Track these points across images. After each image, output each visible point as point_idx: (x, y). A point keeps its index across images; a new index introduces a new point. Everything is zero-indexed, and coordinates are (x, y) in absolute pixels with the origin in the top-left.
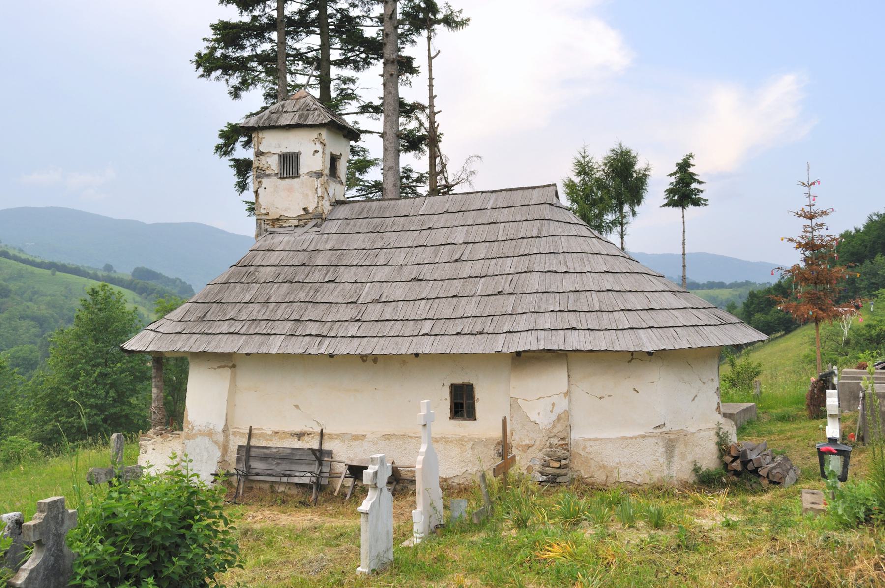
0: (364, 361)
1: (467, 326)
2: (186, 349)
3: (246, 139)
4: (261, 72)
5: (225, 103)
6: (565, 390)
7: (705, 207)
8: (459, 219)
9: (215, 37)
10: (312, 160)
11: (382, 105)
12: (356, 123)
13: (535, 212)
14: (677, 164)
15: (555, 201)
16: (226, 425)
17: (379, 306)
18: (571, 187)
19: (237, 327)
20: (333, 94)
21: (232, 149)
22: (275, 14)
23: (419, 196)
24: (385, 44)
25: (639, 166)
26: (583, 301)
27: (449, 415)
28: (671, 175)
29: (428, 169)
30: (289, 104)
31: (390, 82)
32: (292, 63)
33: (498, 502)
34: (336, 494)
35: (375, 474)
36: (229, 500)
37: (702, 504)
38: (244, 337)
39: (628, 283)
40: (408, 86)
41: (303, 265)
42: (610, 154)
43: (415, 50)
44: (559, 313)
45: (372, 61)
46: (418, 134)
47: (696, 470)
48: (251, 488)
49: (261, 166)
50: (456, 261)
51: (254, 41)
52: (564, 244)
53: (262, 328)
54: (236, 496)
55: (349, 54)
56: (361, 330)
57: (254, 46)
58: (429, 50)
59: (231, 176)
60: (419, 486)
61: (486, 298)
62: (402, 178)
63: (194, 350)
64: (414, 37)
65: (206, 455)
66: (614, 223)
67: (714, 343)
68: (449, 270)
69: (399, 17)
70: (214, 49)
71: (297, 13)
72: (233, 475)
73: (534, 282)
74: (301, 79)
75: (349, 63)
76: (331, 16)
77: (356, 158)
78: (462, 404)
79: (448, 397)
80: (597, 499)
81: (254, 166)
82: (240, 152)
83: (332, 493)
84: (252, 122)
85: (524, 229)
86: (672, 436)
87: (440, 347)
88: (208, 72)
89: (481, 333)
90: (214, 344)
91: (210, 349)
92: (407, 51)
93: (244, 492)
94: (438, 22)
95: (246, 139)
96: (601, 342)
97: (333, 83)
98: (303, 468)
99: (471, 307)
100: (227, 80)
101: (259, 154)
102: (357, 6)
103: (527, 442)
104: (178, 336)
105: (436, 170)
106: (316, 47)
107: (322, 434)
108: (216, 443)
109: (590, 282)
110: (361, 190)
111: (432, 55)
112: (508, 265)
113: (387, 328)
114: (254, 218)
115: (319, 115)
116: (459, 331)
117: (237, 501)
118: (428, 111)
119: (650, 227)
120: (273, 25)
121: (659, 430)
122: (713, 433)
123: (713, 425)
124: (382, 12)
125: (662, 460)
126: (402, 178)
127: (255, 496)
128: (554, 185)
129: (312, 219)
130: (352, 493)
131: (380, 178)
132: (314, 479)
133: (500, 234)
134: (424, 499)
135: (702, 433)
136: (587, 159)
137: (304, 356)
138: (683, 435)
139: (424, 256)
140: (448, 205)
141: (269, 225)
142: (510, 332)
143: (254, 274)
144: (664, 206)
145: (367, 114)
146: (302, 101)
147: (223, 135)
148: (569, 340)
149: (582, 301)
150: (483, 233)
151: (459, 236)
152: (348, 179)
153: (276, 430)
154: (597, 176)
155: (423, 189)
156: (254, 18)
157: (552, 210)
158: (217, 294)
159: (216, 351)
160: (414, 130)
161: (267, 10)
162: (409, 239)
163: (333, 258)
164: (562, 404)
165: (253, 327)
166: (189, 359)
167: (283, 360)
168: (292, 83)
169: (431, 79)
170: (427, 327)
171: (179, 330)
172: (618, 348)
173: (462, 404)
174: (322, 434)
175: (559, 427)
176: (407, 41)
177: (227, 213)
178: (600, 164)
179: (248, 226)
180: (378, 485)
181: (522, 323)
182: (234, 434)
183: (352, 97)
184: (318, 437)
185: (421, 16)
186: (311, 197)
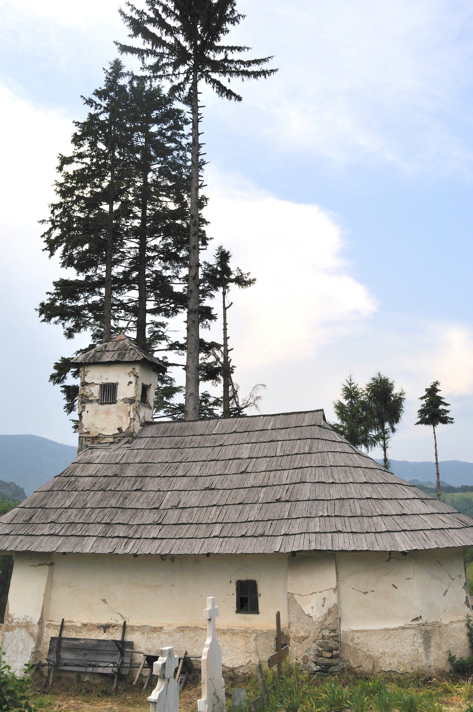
0: (163, 560)
1: (250, 529)
2: (12, 548)
3: (75, 370)
4: (91, 318)
5: (61, 342)
6: (334, 586)
7: (452, 425)
8: (244, 438)
9: (56, 291)
10: (127, 388)
11: (186, 344)
12: (165, 358)
13: (307, 433)
14: (427, 390)
15: (322, 423)
16: (42, 618)
17: (177, 512)
18: (340, 408)
19: (57, 529)
20: (148, 336)
21: (64, 378)
22: (104, 275)
23: (216, 417)
24: (189, 298)
25: (396, 391)
26: (347, 507)
27: (235, 609)
28: (422, 398)
29: (222, 395)
30: (110, 345)
31: (192, 327)
32: (116, 311)
33: (273, 691)
34: (134, 683)
35: (164, 665)
36: (39, 689)
37: (450, 692)
38: (62, 538)
39: (384, 492)
40: (208, 328)
41: (116, 475)
42: (371, 382)
43: (214, 302)
44: (327, 518)
45: (179, 310)
46: (215, 366)
47: (451, 659)
48: (60, 678)
49: (85, 393)
50: (242, 473)
51: (87, 294)
52: (330, 459)
53: (78, 530)
54: (46, 686)
55: (162, 305)
56: (161, 532)
57: (86, 298)
58: (224, 302)
59: (61, 400)
60: (204, 676)
61: (267, 505)
62: (201, 401)
63: (19, 549)
64: (212, 292)
65: (21, 646)
66: (377, 438)
67: (458, 543)
68: (236, 480)
69: (201, 277)
70: (54, 300)
71: (122, 273)
72: (44, 665)
73: (306, 491)
74: (122, 324)
75: (161, 312)
76: (148, 276)
77: (164, 385)
78: (247, 600)
79: (235, 592)
80: (359, 688)
81: (80, 393)
82: (71, 380)
83: (131, 683)
84: (81, 358)
85: (298, 447)
86: (428, 628)
87: (227, 547)
88: (48, 318)
89: (262, 536)
90: (36, 543)
91: (32, 549)
92: (207, 302)
93: (53, 681)
94: (232, 281)
95: (75, 370)
96: (363, 543)
97: (147, 327)
98: (108, 658)
99: (253, 513)
100: (63, 324)
101: (84, 384)
102: (169, 269)
103: (302, 634)
104: (6, 537)
105: (229, 395)
106: (135, 299)
107: (125, 626)
108: (31, 635)
109: (353, 491)
110: (168, 411)
111: (226, 306)
112: (285, 477)
113: (183, 531)
114: (77, 435)
115: (134, 354)
116: (243, 533)
117: (46, 691)
118: (222, 349)
119: (408, 441)
120: (102, 282)
121: (416, 622)
122: (463, 624)
123: (462, 617)
124: (188, 274)
125: (421, 650)
126: (201, 401)
127: (63, 685)
128: (322, 410)
129: (124, 437)
130: (149, 682)
131: (183, 401)
132: (115, 669)
133: (279, 450)
134: (208, 689)
135: (454, 625)
136: (353, 386)
137: (112, 556)
138: (437, 626)
139: (216, 468)
140: (236, 426)
141: (90, 441)
142: (286, 535)
143: (74, 483)
144: (418, 423)
145: (174, 351)
146: (121, 343)
147: (57, 366)
148: (336, 542)
149: (347, 507)
150: (265, 449)
151: (245, 452)
152: (156, 403)
153: (85, 622)
154: (362, 400)
155: (219, 411)
156: (88, 277)
157: (320, 431)
158: (42, 500)
159: (37, 550)
160: (212, 363)
161: (98, 271)
162: (205, 454)
163: (141, 470)
164: (332, 599)
165: (70, 529)
166: (14, 557)
167: (95, 560)
168: (115, 327)
169: (225, 324)
170: (217, 530)
171: (7, 532)
172: (377, 548)
173: (247, 600)
174: (125, 626)
175: (330, 620)
176: (207, 295)
177: (57, 427)
178: (364, 389)
179: (73, 440)
180: (166, 676)
181: (296, 527)
182: (48, 626)
183: (163, 338)
184: (121, 629)
185: (218, 276)
186: (124, 419)
